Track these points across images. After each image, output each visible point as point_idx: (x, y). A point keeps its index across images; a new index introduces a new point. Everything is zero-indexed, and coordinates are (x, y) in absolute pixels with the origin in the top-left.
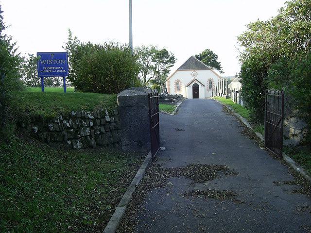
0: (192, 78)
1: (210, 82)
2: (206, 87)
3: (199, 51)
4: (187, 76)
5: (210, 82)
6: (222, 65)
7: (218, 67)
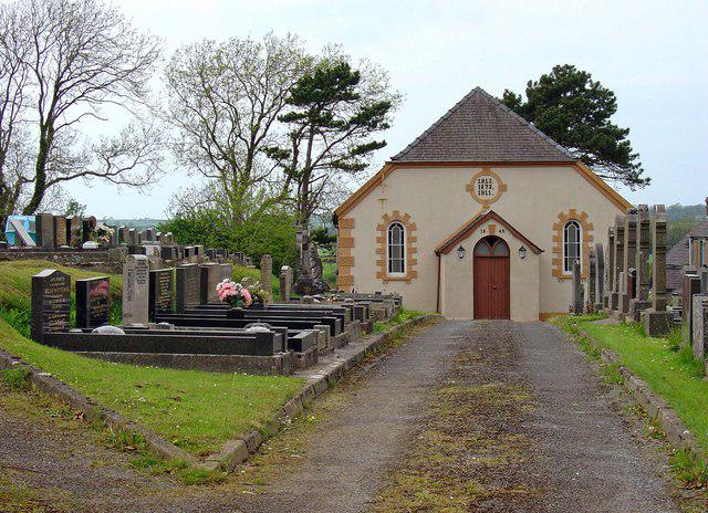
0: (476, 210)
1: (572, 226)
2: (549, 256)
3: (514, 77)
4: (443, 204)
5: (572, 226)
6: (636, 142)
7: (614, 151)
